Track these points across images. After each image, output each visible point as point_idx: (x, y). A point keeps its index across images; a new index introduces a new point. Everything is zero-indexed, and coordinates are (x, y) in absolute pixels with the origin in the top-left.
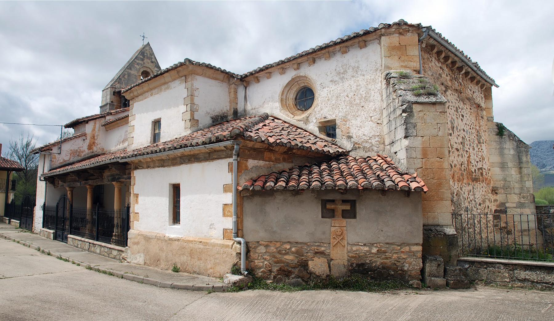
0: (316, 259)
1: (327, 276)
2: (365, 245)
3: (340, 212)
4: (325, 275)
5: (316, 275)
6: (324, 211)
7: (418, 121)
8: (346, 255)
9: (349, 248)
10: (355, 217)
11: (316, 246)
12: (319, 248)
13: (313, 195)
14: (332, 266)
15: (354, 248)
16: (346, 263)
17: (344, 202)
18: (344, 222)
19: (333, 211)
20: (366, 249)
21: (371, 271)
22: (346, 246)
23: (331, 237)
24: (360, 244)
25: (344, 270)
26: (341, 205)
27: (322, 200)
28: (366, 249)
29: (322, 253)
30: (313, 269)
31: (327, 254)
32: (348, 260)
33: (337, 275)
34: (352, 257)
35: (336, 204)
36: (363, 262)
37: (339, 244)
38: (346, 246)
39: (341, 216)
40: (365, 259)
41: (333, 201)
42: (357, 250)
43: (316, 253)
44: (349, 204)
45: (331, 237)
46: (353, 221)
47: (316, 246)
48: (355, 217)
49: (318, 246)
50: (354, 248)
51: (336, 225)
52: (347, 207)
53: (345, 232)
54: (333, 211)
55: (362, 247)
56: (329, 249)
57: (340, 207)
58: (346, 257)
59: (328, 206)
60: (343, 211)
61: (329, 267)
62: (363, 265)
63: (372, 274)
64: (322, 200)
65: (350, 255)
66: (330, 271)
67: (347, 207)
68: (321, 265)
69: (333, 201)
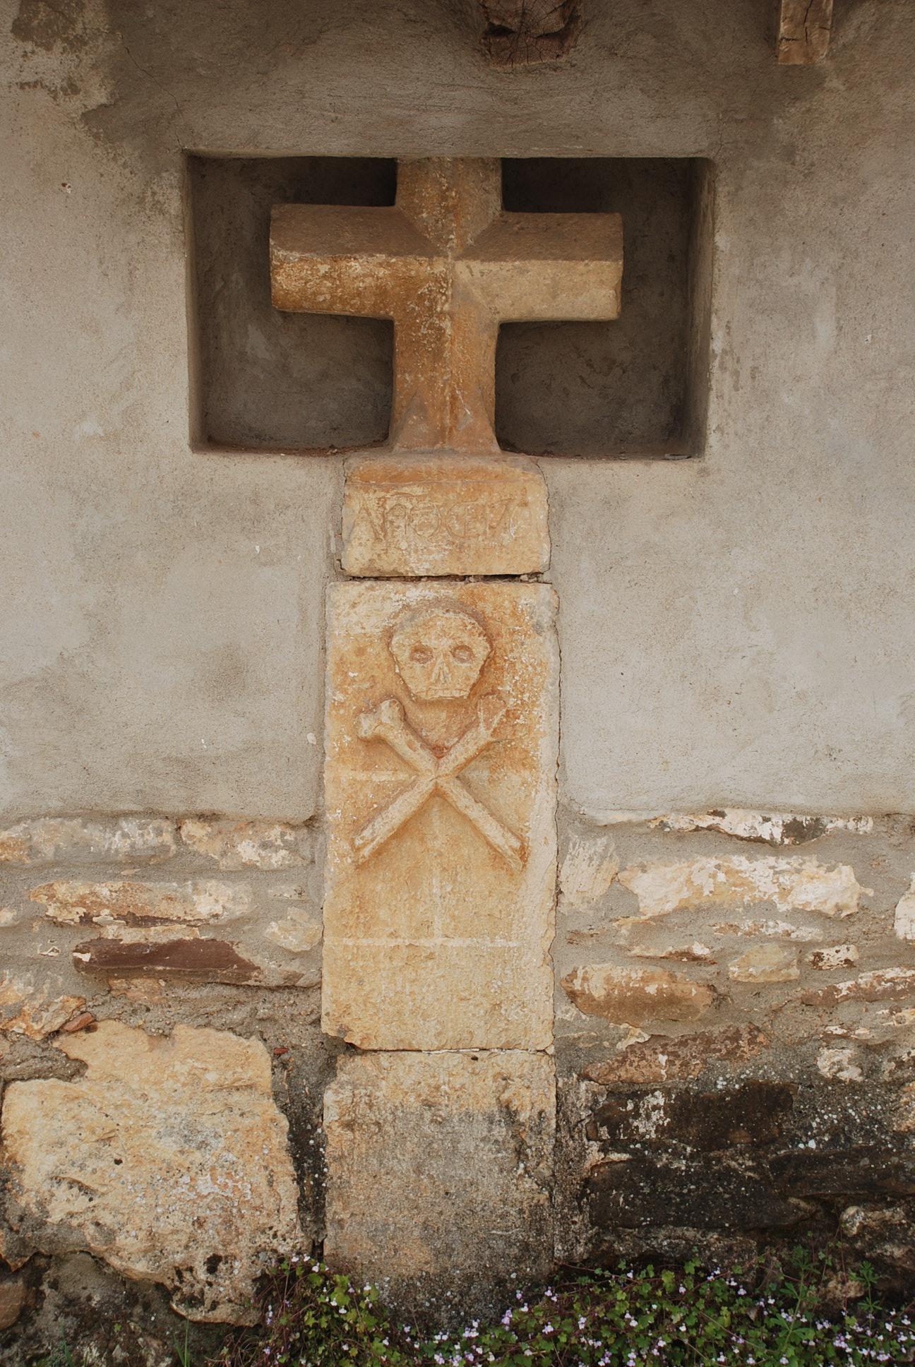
0: (112, 1049)
1: (277, 1284)
2: (802, 833)
3: (469, 360)
4: (240, 1274)
5: (121, 1279)
6: (256, 342)
7: (59, 1108)
8: (537, 986)
9: (585, 878)
10: (675, 428)
11: (107, 865)
12: (154, 895)
13: (50, 63)
14: (335, 1138)
15: (659, 887)
16: (535, 1096)
17: (541, 192)
18: (529, 506)
19: (373, 340)
20: (826, 885)
21: (873, 1192)
22: (543, 855)
23: (337, 735)
24: (738, 823)
25: (501, 1190)
26: (488, 246)
27: (200, 167)
28: (826, 885)
29: (204, 963)
30: (64, 1205)
31: (271, 970)
32: (569, 1057)
33: (415, 1258)
34: (632, 1005)
35: (416, 242)
36: (762, 1065)
37: (439, 829)
38: (543, 855)
39: (476, 419)
40: (801, 1024)
41: (364, 187)
42: (691, 913)
43: (115, 963)
44: (606, 226)
45: (337, 735)
46: (642, 485)
47: (107, 865)
48: (675, 428)
49: (146, 865)
50: (659, 887)
51: (324, 570)
52: (577, 284)
53: (532, 653)
54: (373, 340)
55: (760, 873)
56: (308, 900)
57: (468, 272)
58: (537, 1016)
59: (300, 272)
60: (515, 336)
61: (305, 1149)
62: (764, 1104)
63: (887, 1232)
64: (200, 167)
65: (599, 977)
66: (312, 1204)
67: (577, 284)
68: (191, 1136)
69: (364, 187)
